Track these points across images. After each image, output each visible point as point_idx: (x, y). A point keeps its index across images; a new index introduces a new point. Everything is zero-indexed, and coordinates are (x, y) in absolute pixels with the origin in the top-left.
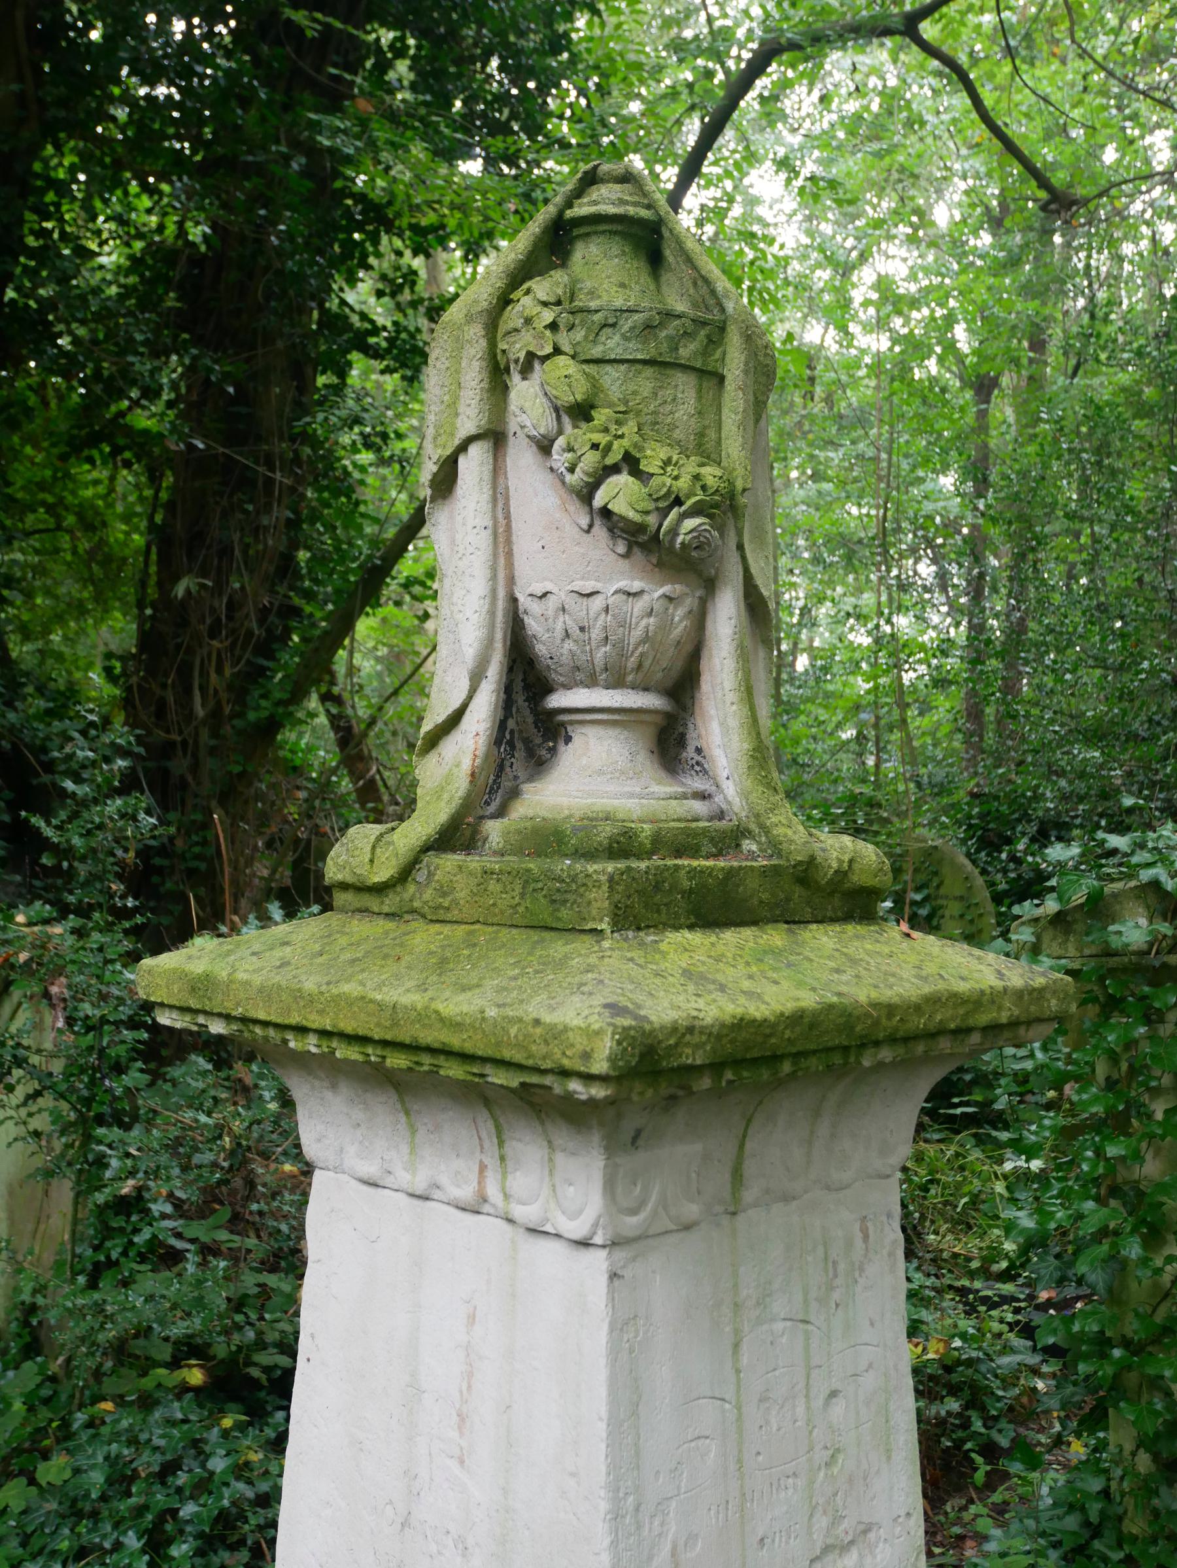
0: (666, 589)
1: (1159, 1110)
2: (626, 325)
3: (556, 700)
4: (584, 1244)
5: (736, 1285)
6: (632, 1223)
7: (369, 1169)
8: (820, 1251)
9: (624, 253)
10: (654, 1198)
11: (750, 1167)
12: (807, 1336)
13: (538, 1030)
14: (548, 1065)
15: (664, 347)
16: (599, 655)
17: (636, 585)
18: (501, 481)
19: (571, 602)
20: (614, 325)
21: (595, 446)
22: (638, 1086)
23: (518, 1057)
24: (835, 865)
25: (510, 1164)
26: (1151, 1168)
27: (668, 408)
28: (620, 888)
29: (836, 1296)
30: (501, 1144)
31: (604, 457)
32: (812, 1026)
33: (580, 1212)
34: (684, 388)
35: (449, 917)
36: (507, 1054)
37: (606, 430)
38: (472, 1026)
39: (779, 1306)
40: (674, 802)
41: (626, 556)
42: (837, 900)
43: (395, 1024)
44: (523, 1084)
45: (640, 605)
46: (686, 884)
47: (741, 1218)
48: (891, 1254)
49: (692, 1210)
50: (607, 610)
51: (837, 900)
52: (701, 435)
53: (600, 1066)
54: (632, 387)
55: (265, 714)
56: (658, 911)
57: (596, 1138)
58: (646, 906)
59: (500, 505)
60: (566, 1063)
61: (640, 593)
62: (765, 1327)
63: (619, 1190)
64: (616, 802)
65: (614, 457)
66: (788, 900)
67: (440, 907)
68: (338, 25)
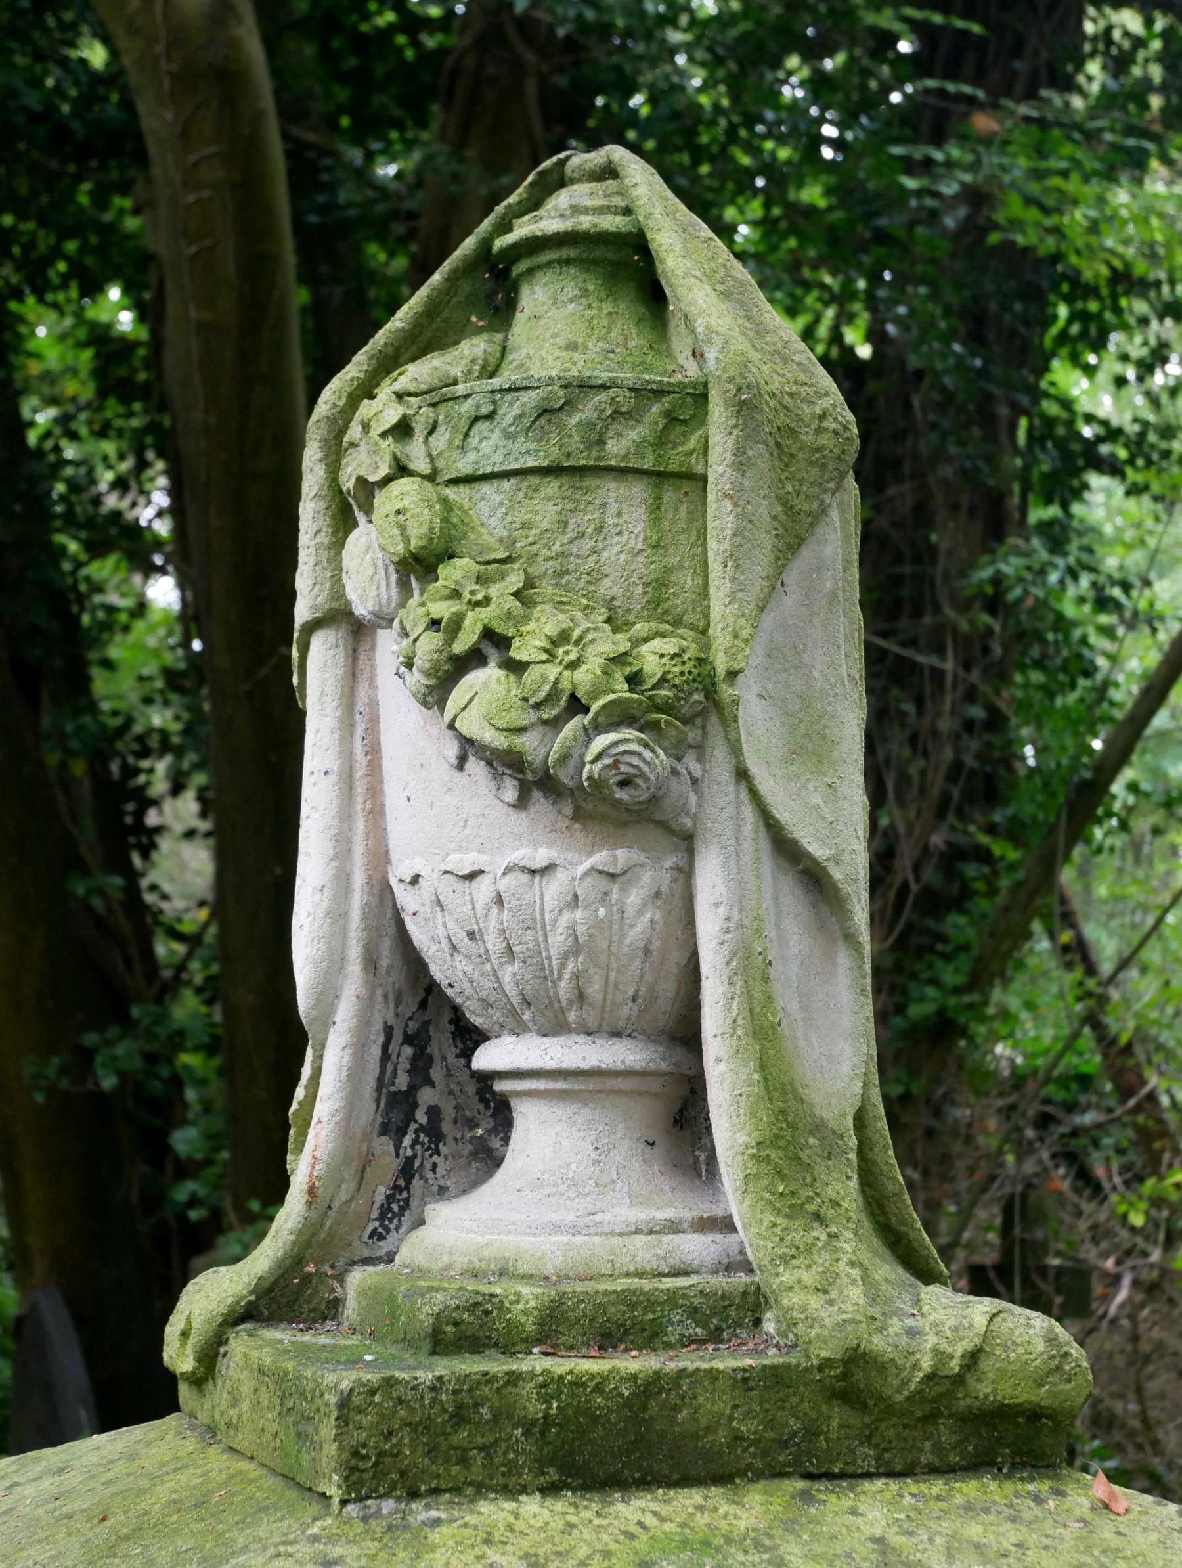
0: (600, 858)
2: (510, 411)
3: (486, 1058)
9: (585, 293)
15: (576, 441)
16: (508, 973)
17: (541, 857)
18: (362, 692)
19: (448, 889)
20: (490, 416)
21: (435, 624)
24: (926, 1364)
27: (587, 544)
28: (366, 1420)
31: (450, 641)
34: (624, 511)
37: (456, 594)
40: (640, 1239)
41: (522, 803)
42: (945, 1432)
45: (554, 889)
46: (535, 1409)
50: (499, 900)
51: (945, 1432)
52: (661, 583)
54: (521, 516)
55: (929, 1008)
56: (464, 1461)
58: (432, 1451)
59: (359, 732)
61: (547, 870)
64: (526, 1241)
65: (465, 641)
66: (812, 1433)
68: (937, 19)
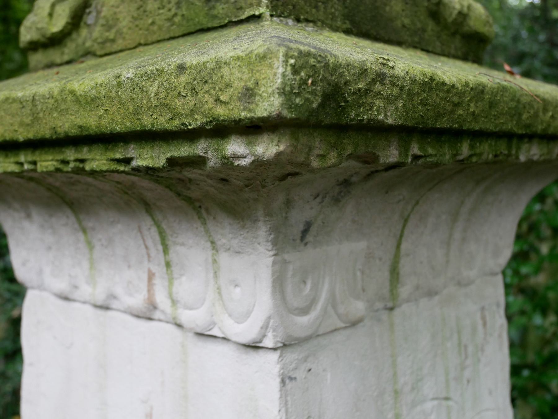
1: (545, 249)
4: (254, 347)
5: (395, 374)
6: (303, 323)
7: (61, 285)
8: (455, 336)
10: (324, 296)
11: (405, 266)
12: (449, 410)
13: (183, 79)
14: (197, 121)
22: (319, 146)
23: (160, 121)
25: (175, 270)
26: (541, 279)
29: (467, 373)
30: (166, 250)
32: (492, 104)
33: (248, 314)
35: (115, 47)
36: (147, 121)
38: (107, 96)
39: (429, 388)
43: (36, 119)
44: (172, 162)
47: (397, 312)
48: (500, 336)
49: (359, 307)
53: (269, 105)
57: (262, 231)
60: (221, 112)
62: (419, 408)
63: (289, 289)
67: (107, 40)
